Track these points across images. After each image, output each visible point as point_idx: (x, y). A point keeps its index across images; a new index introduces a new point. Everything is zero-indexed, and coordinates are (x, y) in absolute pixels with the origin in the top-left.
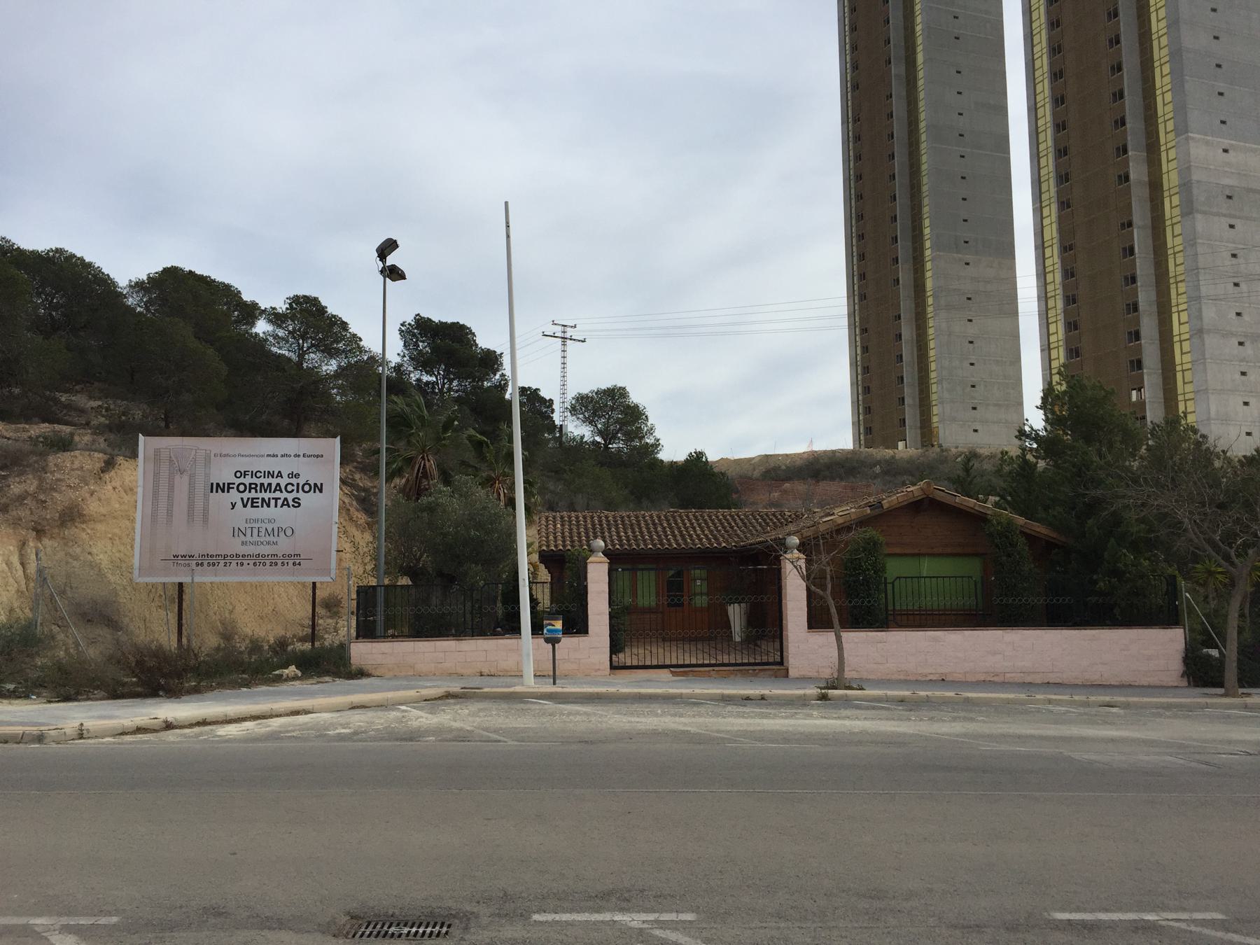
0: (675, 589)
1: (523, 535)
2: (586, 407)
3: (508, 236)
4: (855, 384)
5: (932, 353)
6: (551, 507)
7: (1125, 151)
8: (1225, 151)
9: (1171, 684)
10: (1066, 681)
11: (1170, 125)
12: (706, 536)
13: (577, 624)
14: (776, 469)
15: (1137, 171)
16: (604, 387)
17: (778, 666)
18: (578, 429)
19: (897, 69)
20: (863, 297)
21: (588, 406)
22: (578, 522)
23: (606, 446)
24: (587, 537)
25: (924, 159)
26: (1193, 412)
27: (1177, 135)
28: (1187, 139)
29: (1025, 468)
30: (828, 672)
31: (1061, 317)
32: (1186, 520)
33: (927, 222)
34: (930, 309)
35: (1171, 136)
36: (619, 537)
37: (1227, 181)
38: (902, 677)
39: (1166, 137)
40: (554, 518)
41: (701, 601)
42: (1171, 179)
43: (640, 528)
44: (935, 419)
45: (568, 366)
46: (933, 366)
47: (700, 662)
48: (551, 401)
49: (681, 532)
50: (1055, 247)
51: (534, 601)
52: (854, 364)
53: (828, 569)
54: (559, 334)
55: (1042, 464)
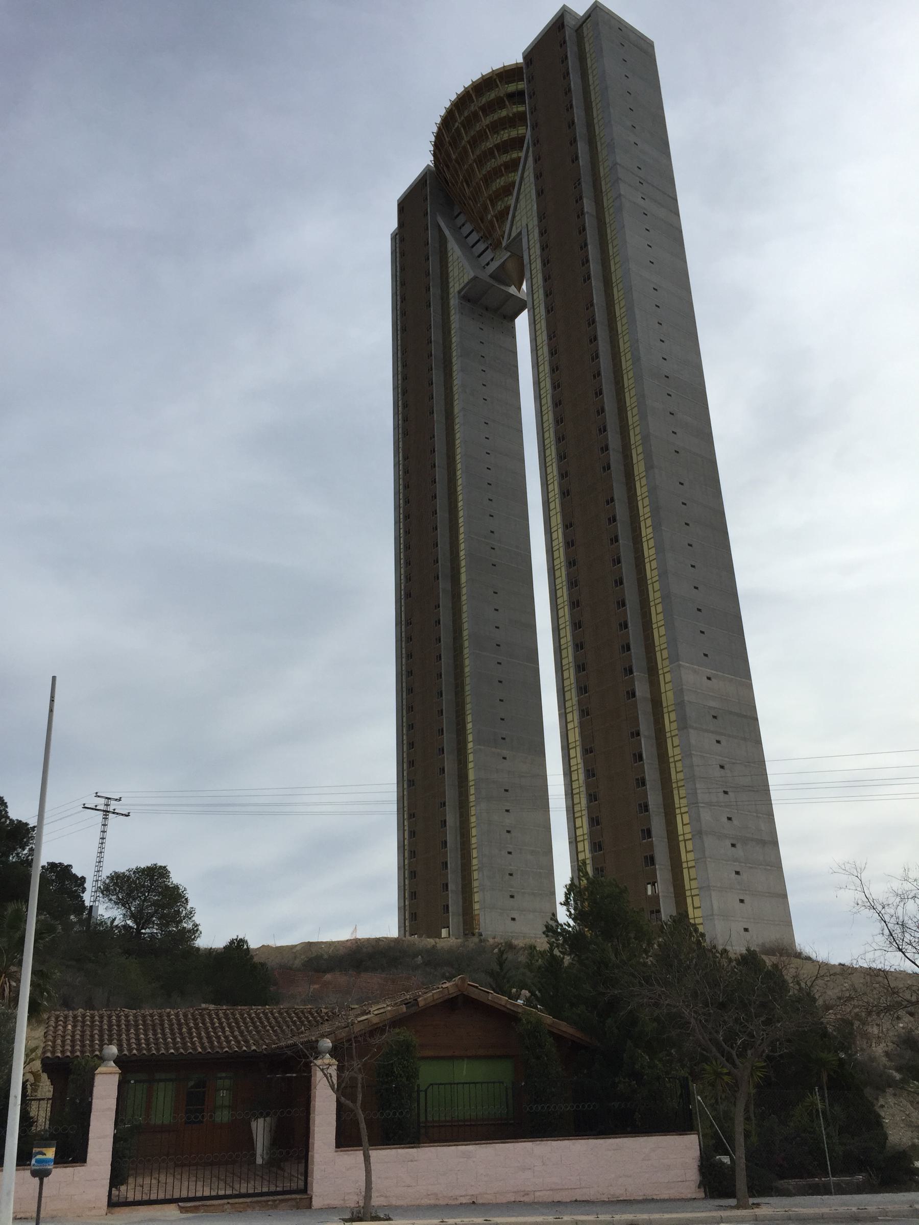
0: (195, 1102)
1: (23, 1034)
2: (121, 888)
3: (51, 711)
4: (401, 868)
5: (474, 840)
6: (67, 1004)
7: (631, 672)
8: (709, 678)
9: (689, 1196)
10: (592, 1198)
11: (665, 654)
12: (235, 1037)
13: (73, 1152)
14: (319, 958)
15: (642, 690)
16: (143, 865)
17: (299, 1195)
18: (108, 912)
19: (444, 585)
20: (411, 783)
21: (121, 886)
22: (93, 1021)
23: (138, 931)
24: (101, 1040)
25: (467, 662)
26: (695, 915)
27: (671, 663)
28: (679, 666)
29: (553, 963)
30: (354, 1200)
31: (585, 813)
32: (693, 1021)
33: (469, 718)
34: (472, 798)
35: (666, 663)
36: (138, 1039)
37: (712, 704)
38: (432, 1202)
39: (662, 664)
40: (66, 1017)
41: (223, 1116)
42: (668, 698)
43: (163, 1030)
44: (476, 906)
45: (107, 841)
46: (475, 853)
47: (214, 1193)
48: (83, 879)
49: (208, 1033)
50: (578, 749)
51: (26, 1120)
52: (401, 847)
53: (360, 1077)
54: (102, 807)
55: (567, 960)
